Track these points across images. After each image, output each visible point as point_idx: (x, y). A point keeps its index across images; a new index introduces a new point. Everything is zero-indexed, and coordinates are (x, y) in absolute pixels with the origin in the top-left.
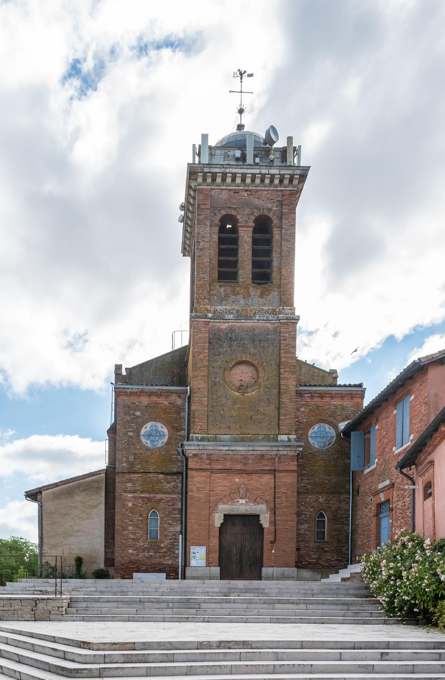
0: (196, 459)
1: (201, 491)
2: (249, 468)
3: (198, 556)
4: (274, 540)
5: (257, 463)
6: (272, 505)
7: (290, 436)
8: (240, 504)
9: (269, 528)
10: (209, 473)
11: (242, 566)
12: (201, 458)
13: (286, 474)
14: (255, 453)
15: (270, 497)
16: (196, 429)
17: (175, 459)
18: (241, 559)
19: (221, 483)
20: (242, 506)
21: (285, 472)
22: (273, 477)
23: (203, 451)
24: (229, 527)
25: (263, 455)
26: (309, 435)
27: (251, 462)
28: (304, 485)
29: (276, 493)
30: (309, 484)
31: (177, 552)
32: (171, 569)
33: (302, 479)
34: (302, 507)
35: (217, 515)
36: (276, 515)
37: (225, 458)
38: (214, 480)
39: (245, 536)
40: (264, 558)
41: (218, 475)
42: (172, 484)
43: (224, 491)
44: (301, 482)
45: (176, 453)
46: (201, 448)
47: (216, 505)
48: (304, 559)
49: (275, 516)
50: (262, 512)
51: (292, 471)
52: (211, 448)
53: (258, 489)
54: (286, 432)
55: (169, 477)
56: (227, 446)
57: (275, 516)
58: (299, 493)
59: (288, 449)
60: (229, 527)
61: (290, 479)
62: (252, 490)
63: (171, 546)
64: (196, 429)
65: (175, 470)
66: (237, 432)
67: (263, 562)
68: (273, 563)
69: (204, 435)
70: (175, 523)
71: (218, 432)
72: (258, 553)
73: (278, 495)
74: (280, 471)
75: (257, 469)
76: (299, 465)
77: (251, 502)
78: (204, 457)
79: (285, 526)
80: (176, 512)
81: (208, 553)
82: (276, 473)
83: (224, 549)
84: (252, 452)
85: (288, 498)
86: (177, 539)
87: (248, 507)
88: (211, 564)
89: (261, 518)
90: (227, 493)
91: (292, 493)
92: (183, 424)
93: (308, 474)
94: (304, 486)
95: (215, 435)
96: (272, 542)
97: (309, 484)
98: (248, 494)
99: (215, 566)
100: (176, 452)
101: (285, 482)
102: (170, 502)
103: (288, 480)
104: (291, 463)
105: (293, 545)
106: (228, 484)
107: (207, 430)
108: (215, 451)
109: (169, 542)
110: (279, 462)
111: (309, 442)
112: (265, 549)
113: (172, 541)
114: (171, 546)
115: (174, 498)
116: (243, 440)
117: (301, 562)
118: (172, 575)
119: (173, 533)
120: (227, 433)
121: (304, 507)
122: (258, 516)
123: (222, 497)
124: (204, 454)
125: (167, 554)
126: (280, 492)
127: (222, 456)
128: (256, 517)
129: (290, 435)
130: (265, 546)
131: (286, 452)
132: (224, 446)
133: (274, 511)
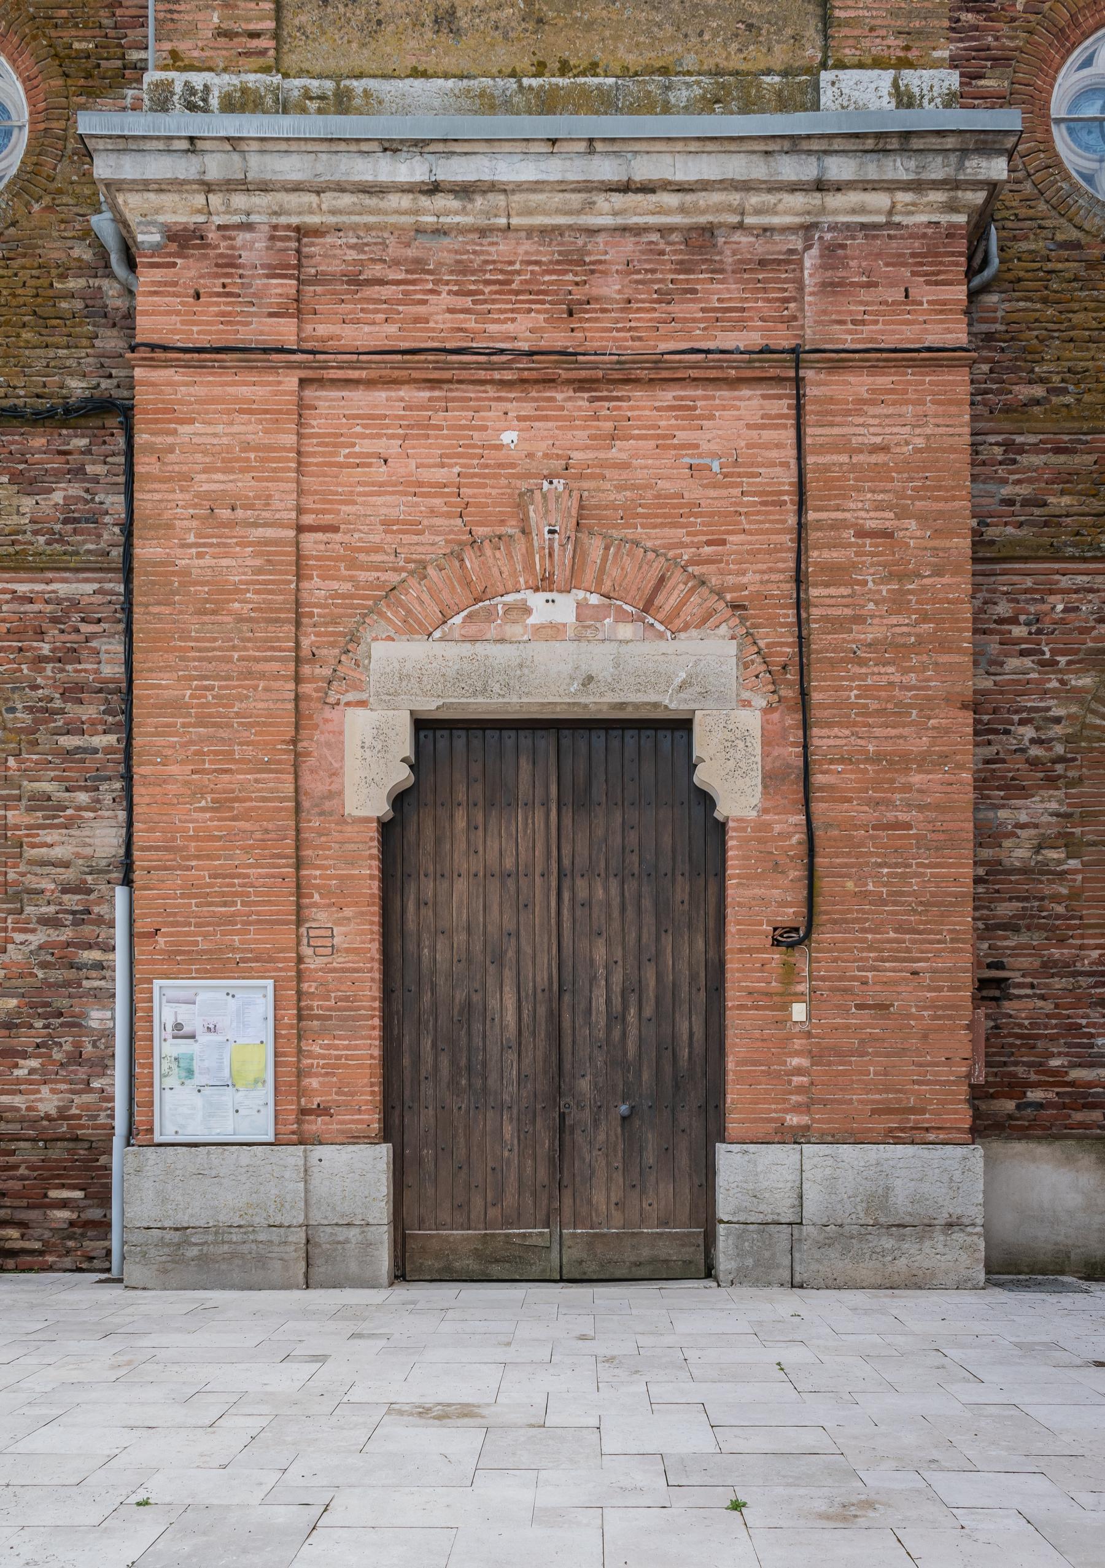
0: (189, 270)
1: (232, 524)
2: (601, 336)
3: (214, 1062)
4: (801, 922)
5: (665, 298)
6: (779, 638)
7: (912, 79)
8: (538, 629)
9: (767, 826)
10: (291, 381)
11: (562, 1128)
12: (230, 263)
13: (884, 381)
14: (640, 210)
15: (764, 576)
16: (192, 31)
17: (78, 305)
18: (559, 1076)
19: (389, 459)
20: (555, 652)
21: (874, 368)
22: (783, 406)
23: (239, 200)
24: (461, 823)
25: (709, 231)
26: (1058, 107)
27: (611, 288)
28: (1024, 490)
29: (813, 536)
30: (1065, 480)
31: (96, 1018)
32: (58, 1152)
33: (1008, 445)
34: (1013, 663)
35: (358, 725)
36: (816, 714)
37: (418, 265)
38: (335, 441)
39: (582, 894)
40: (731, 1065)
41: (361, 399)
42: (58, 497)
43: (413, 527)
44: (1001, 471)
45: (87, 256)
46: (215, 166)
47: (354, 638)
48: (1039, 1067)
49: (806, 726)
50: (705, 694)
51: (931, 357)
52: (290, 167)
53: (673, 511)
54: (876, 47)
55: (39, 442)
56: (419, 145)
57: (806, 726)
58: (986, 554)
59: (899, 168)
60: (461, 823)
61: (920, 421)
62: (629, 515)
63: (57, 975)
64: (192, 31)
65: (77, 387)
66: (503, 56)
67: (722, 1093)
68: (796, 1109)
69: (252, 79)
70: (83, 797)
71: (361, 59)
72: (688, 1026)
73: (827, 555)
74: (840, 360)
75: (663, 346)
76: (989, 337)
77: (622, 617)
78: (254, 249)
79: (888, 803)
80: (89, 711)
81: (296, 1024)
82: (808, 374)
83: (427, 998)
84: (618, 199)
85: (902, 577)
86: (100, 921)
87: (598, 658)
88: (316, 1125)
89: (704, 743)
90: (432, 544)
91: (938, 533)
92: (133, 35)
93: (1056, 410)
94: (1026, 502)
95: (337, 77)
96: (791, 938)
97: (1065, 480)
98: (595, 548)
99: (354, 1139)
100: (83, 253)
101: (875, 449)
102: (40, 633)
103: (905, 432)
104: (926, 294)
105: (953, 962)
106: (440, 475)
107: (276, 36)
108: (329, 200)
109: (36, 939)
110: (829, 288)
111: (1059, 164)
112: (733, 996)
113: (66, 934)
114: (57, 975)
115: (74, 603)
116: (548, 103)
117: (1015, 1088)
118: (64, 1204)
119: (68, 875)
120: (428, 62)
121: (1027, 662)
122: (683, 726)
123: (393, 578)
124: (248, 227)
125: (24, 1040)
126: (842, 525)
127: (394, 250)
128: (667, 734)
129: (911, 65)
130: (732, 965)
131: (881, 200)
132: (390, 147)
133: (796, 682)
